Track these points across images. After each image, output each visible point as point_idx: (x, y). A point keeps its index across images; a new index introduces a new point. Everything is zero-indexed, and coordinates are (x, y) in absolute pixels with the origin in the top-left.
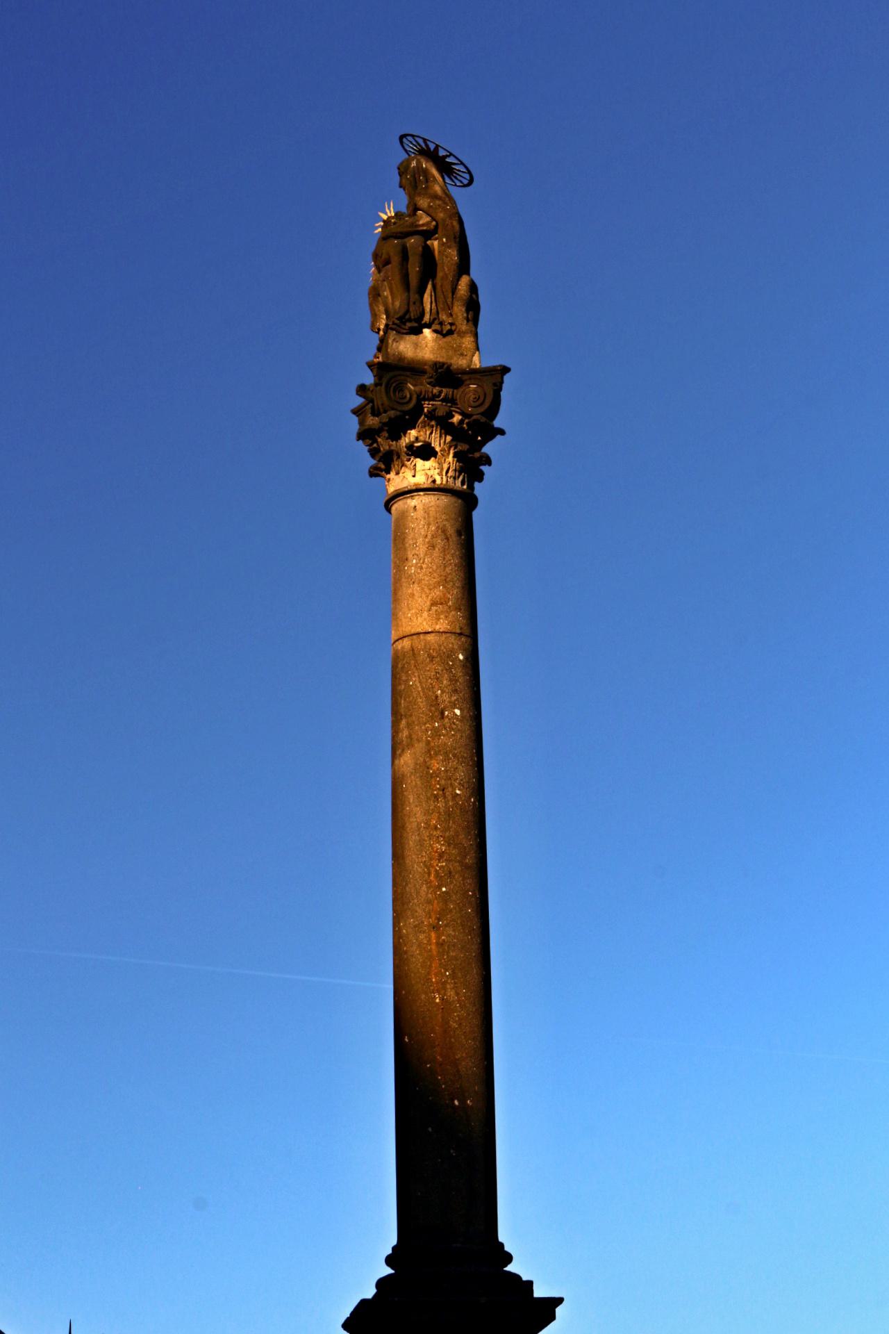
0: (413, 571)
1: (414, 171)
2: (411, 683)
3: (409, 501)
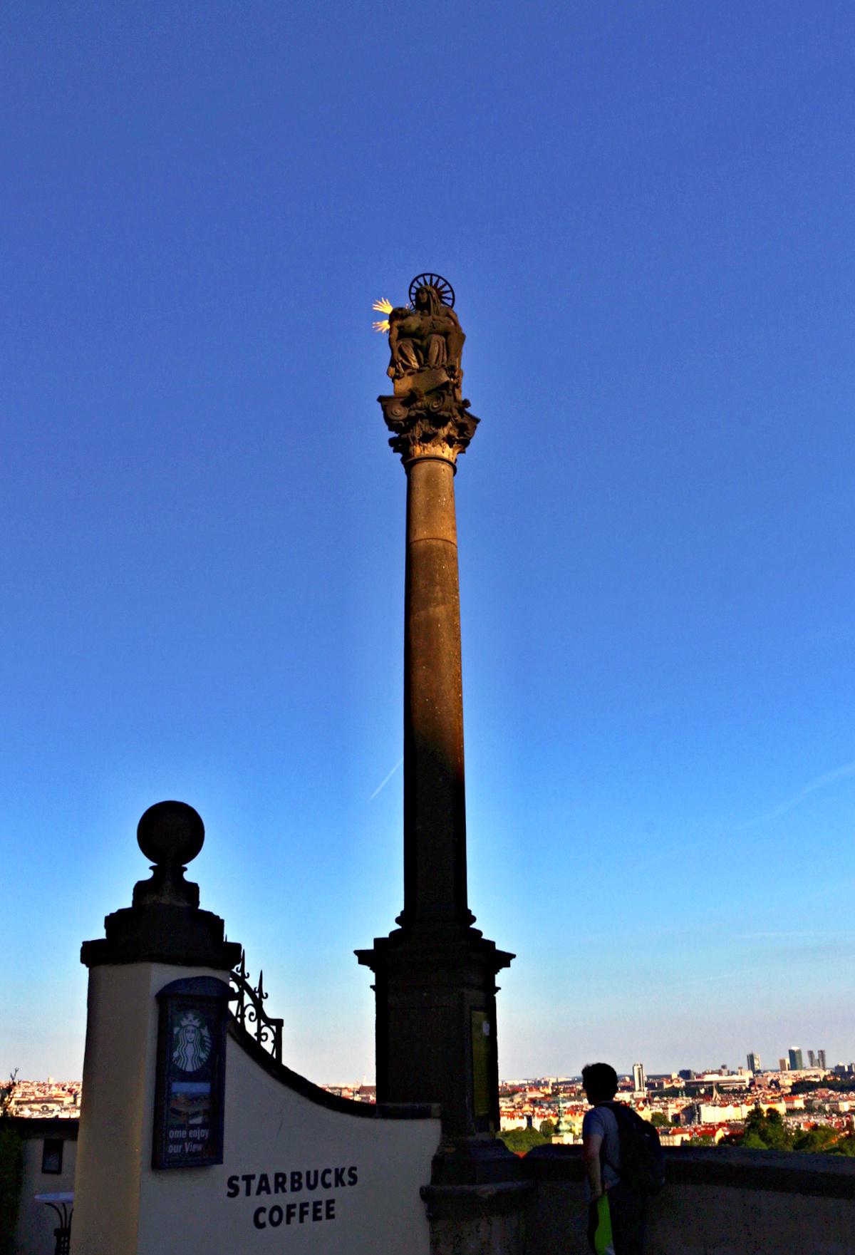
3: (440, 464)
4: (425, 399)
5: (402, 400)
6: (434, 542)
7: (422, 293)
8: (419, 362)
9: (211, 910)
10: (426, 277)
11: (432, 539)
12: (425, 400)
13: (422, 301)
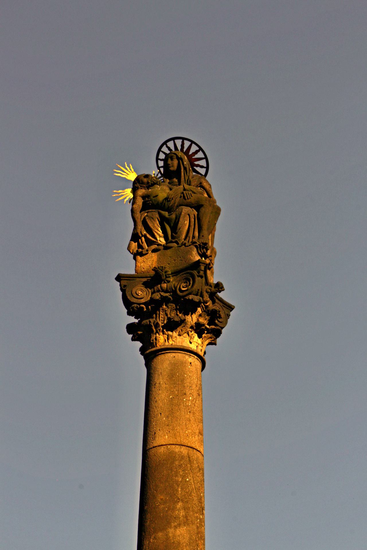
0: (190, 404)
1: (154, 221)
2: (188, 480)
3: (187, 357)
5: (145, 280)
6: (177, 449)
8: (166, 237)
11: (173, 444)
13: (172, 169)
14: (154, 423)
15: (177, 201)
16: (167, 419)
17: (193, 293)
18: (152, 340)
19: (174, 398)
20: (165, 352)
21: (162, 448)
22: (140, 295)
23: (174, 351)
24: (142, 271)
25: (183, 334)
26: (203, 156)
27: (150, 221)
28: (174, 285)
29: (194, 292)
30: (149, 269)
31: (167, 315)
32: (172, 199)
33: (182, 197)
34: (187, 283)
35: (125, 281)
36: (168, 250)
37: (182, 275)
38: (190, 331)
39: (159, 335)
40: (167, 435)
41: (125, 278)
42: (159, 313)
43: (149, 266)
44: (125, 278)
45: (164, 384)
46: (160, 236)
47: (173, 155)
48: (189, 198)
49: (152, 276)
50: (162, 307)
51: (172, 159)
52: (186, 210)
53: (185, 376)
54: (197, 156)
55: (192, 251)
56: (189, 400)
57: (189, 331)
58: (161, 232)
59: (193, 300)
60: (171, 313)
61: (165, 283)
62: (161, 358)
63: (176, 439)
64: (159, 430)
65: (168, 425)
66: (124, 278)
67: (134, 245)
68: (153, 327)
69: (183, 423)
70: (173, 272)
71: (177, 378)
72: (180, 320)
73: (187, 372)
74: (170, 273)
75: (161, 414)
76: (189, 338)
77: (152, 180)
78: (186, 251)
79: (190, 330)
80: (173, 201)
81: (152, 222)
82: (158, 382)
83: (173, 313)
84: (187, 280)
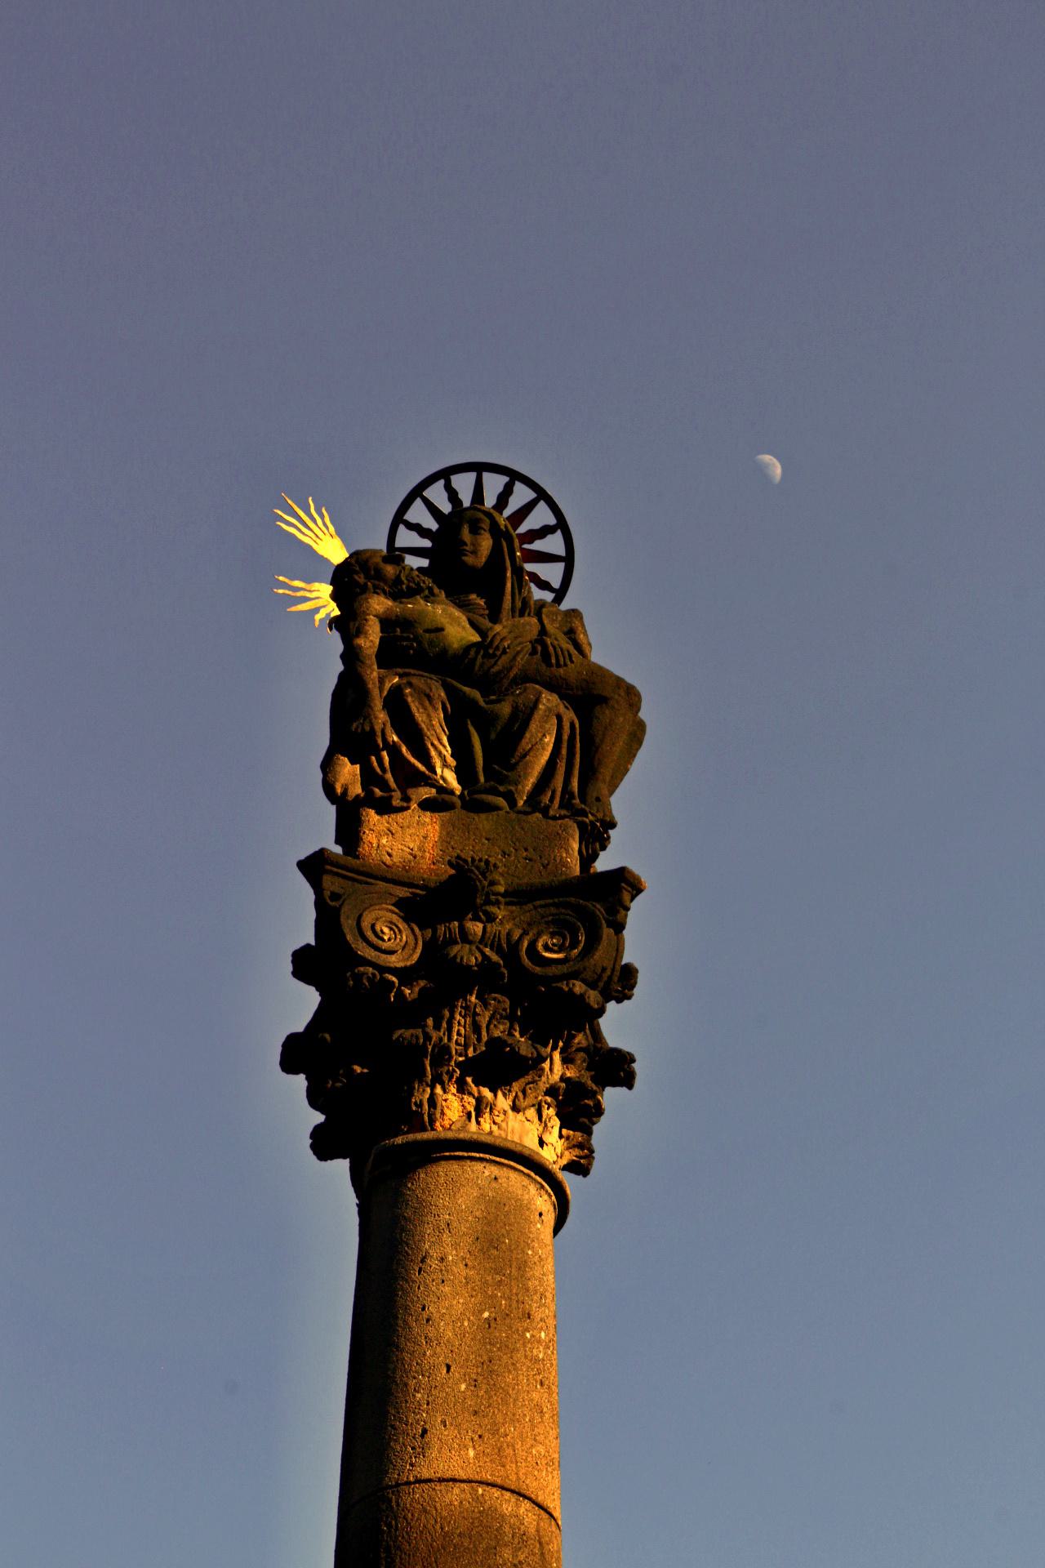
0: (541, 1356)
1: (434, 707)
3: (533, 1189)
4: (500, 913)
5: (403, 892)
6: (508, 1505)
7: (475, 530)
8: (464, 771)
9: (285, 1036)
10: (488, 477)
11: (493, 1485)
12: (505, 921)
13: (469, 560)
14: (419, 1395)
15: (521, 660)
16: (472, 1388)
17: (583, 976)
18: (416, 1103)
19: (495, 1319)
20: (466, 1154)
21: (456, 1491)
22: (386, 938)
23: (498, 1159)
24: (385, 864)
25: (524, 1109)
26: (561, 551)
27: (417, 704)
28: (509, 934)
29: (588, 975)
30: (410, 862)
31: (476, 1028)
32: (504, 652)
33: (538, 656)
34: (564, 939)
35: (336, 878)
36: (483, 816)
37: (541, 906)
38: (546, 1103)
39: (445, 1091)
40: (474, 1448)
41: (340, 871)
42: (452, 1017)
43: (408, 850)
44: (340, 871)
45: (462, 1266)
46: (445, 760)
47: (481, 516)
48: (562, 663)
49: (432, 885)
50: (465, 1000)
51: (475, 530)
52: (549, 700)
53: (527, 1254)
54: (538, 545)
55: (571, 839)
56: (539, 1341)
57: (543, 1104)
58: (450, 752)
59: (585, 999)
60: (492, 1026)
61: (476, 918)
62: (445, 1171)
63: (504, 1466)
64: (444, 1423)
65: (476, 1413)
66: (335, 870)
67: (348, 772)
68: (427, 1058)
69: (525, 1415)
70: (510, 889)
71: (505, 1252)
72: (535, 1055)
73: (534, 1241)
74: (501, 889)
75: (448, 1367)
76: (541, 1129)
77: (412, 578)
78: (546, 834)
79: (549, 1099)
80: (504, 658)
81: (425, 709)
82: (435, 1254)
83: (501, 1027)
84: (562, 928)
